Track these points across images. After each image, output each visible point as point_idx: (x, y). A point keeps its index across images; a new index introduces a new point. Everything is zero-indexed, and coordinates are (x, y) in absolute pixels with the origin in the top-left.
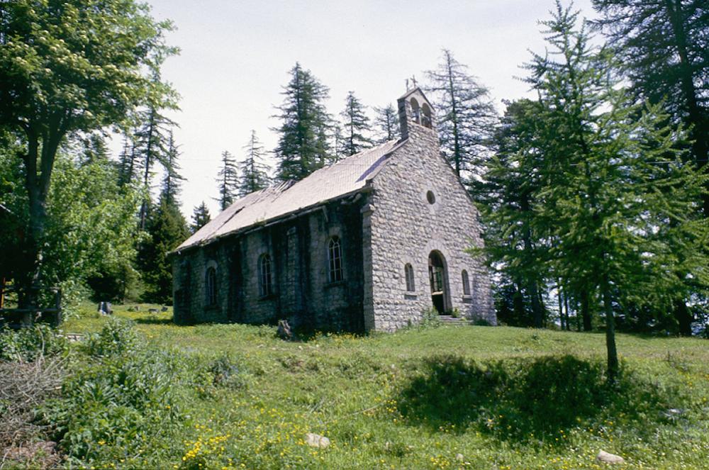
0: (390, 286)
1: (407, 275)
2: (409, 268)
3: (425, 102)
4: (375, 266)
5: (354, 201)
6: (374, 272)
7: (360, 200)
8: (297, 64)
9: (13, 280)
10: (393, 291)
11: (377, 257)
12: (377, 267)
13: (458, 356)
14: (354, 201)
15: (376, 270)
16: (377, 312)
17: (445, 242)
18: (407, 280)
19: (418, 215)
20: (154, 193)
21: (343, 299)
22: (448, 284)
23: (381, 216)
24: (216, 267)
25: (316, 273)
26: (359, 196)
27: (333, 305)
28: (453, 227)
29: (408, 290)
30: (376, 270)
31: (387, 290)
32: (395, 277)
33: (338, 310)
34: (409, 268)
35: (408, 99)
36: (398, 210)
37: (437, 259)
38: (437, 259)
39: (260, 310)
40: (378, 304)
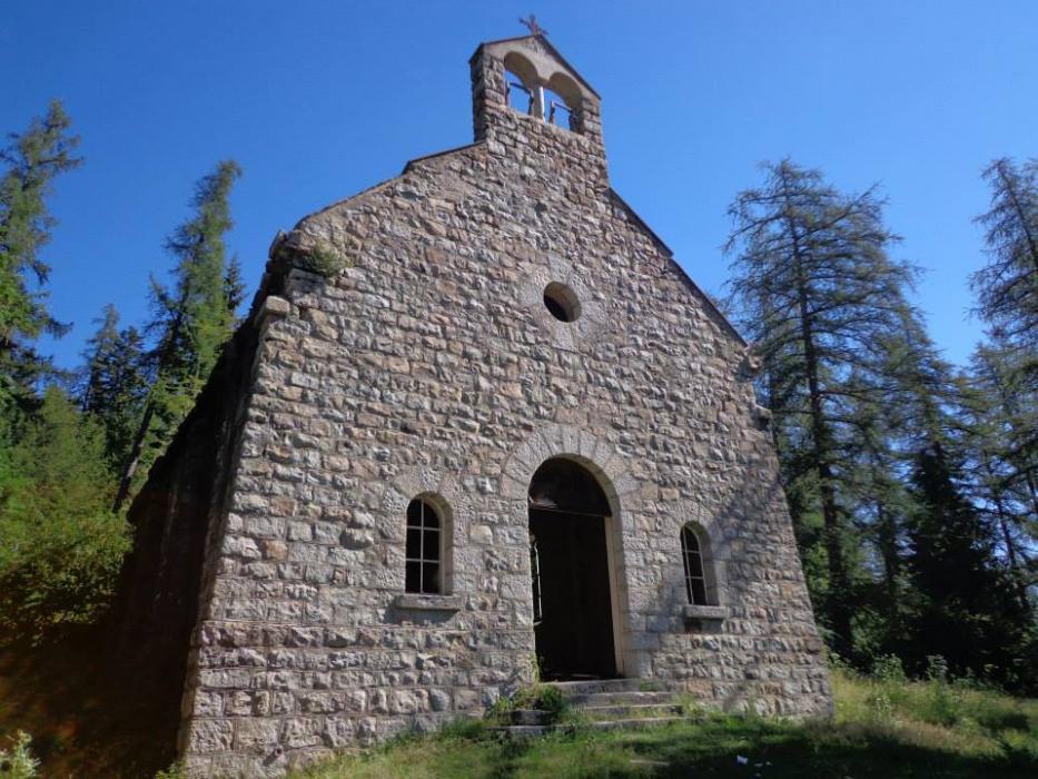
1: (412, 537)
2: (426, 520)
3: (561, 69)
8: (72, 324)
9: (969, 669)
10: (328, 593)
11: (265, 466)
12: (257, 501)
16: (208, 678)
17: (613, 435)
18: (412, 550)
19: (497, 346)
21: (988, 524)
23: (315, 334)
24: (293, 657)
28: (649, 393)
29: (412, 586)
30: (250, 512)
32: (347, 541)
34: (426, 520)
36: (406, 320)
40: (228, 644)
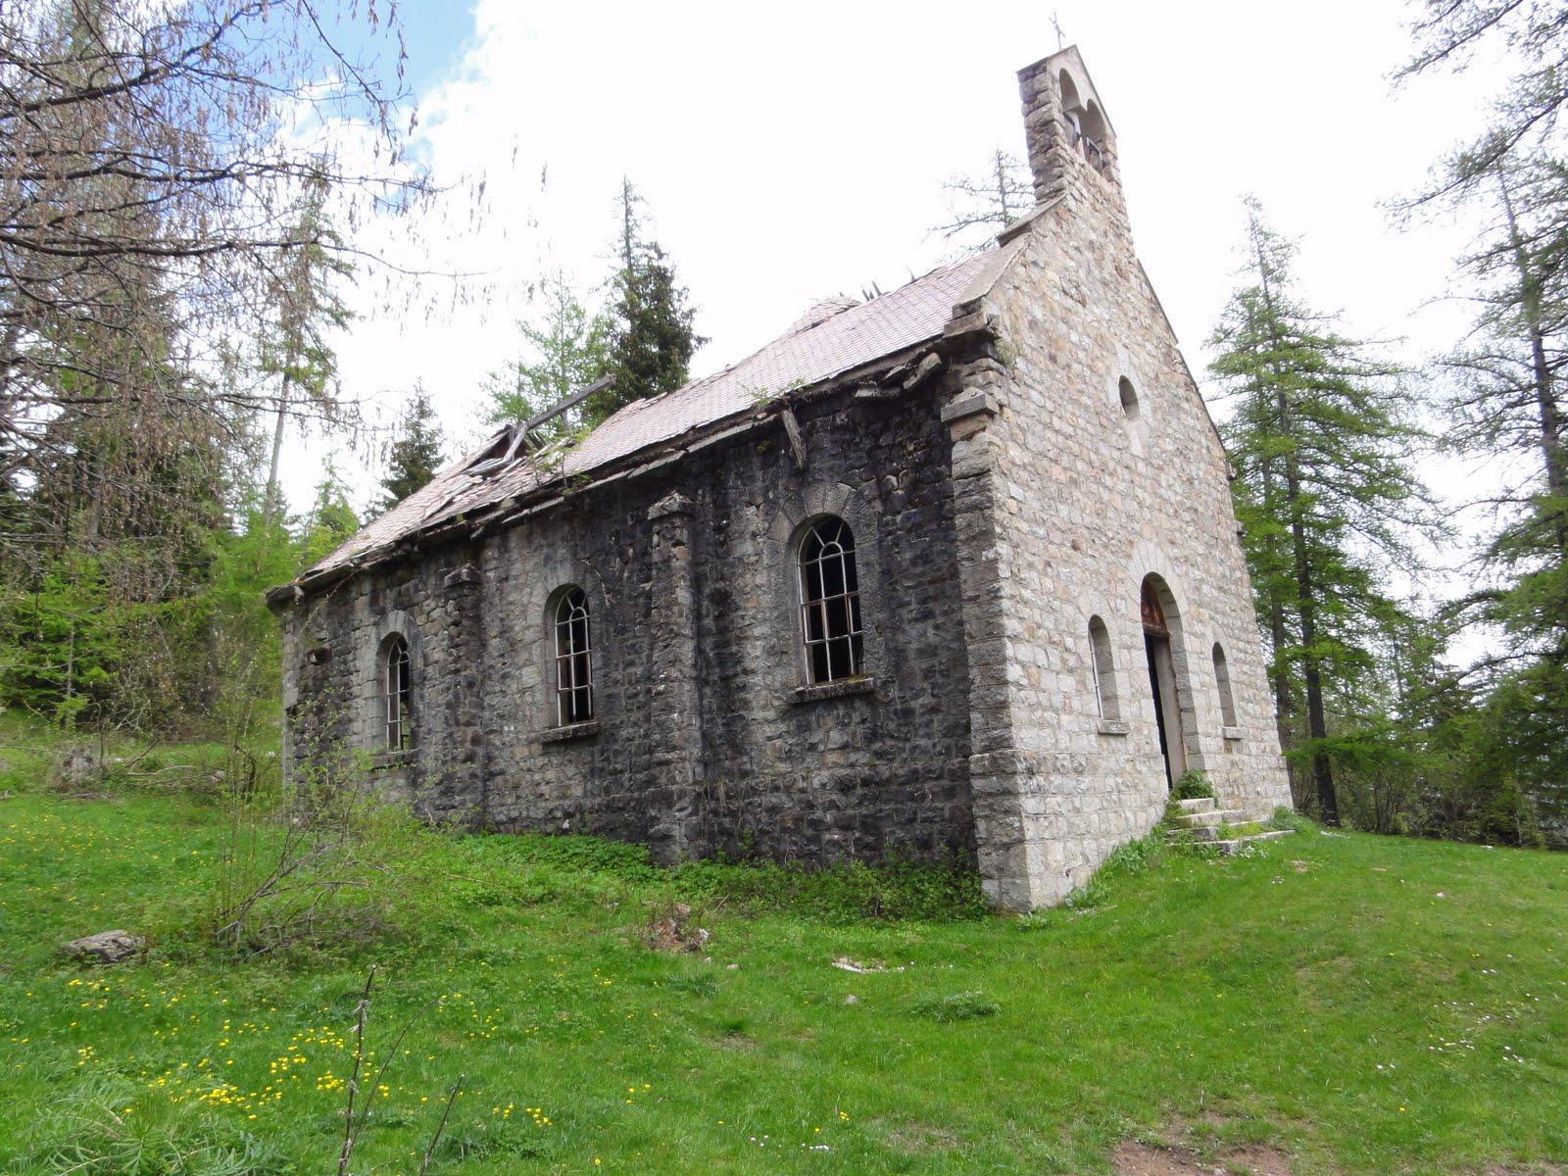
0: (1057, 701)
2: (1097, 627)
4: (1011, 625)
5: (908, 384)
6: (1010, 650)
7: (936, 376)
10: (1065, 718)
13: (358, 664)
14: (908, 384)
15: (1015, 638)
20: (444, 96)
22: (1188, 690)
25: (754, 652)
26: (933, 359)
27: (823, 765)
30: (1015, 638)
31: (1049, 715)
33: (845, 787)
34: (1097, 627)
35: (1055, 69)
37: (1154, 593)
38: (1154, 593)
39: (551, 775)
